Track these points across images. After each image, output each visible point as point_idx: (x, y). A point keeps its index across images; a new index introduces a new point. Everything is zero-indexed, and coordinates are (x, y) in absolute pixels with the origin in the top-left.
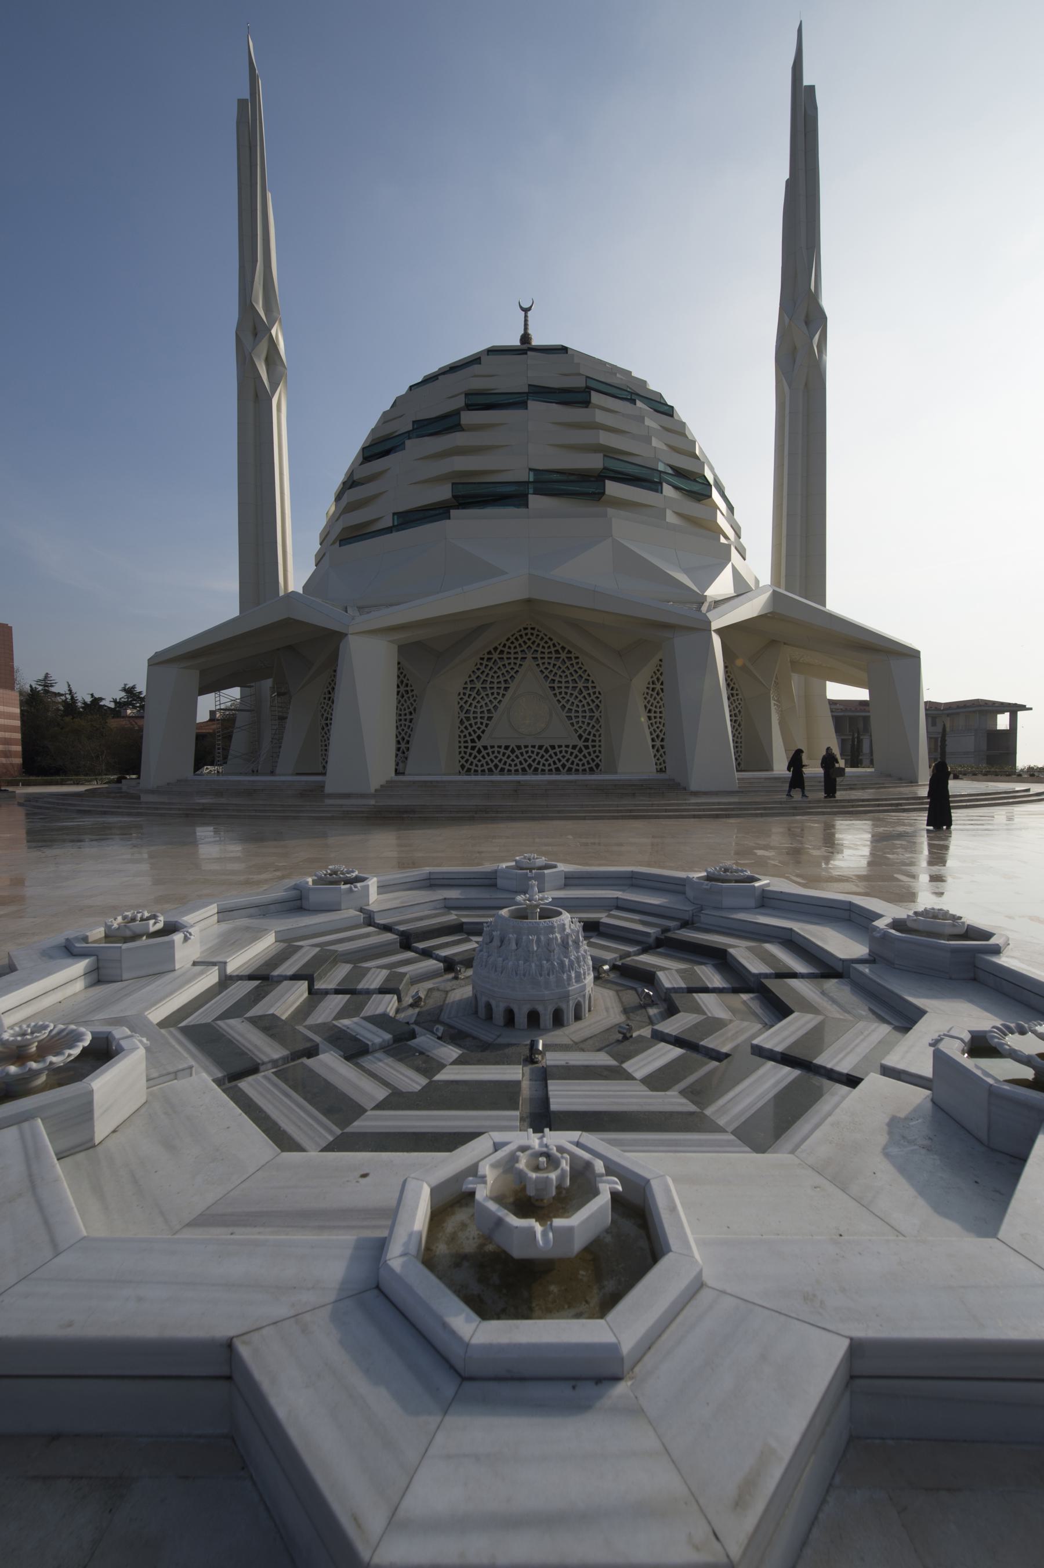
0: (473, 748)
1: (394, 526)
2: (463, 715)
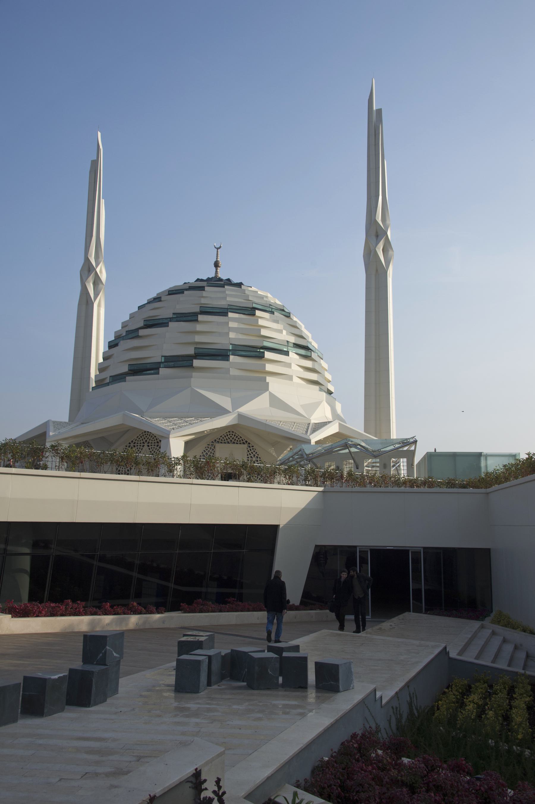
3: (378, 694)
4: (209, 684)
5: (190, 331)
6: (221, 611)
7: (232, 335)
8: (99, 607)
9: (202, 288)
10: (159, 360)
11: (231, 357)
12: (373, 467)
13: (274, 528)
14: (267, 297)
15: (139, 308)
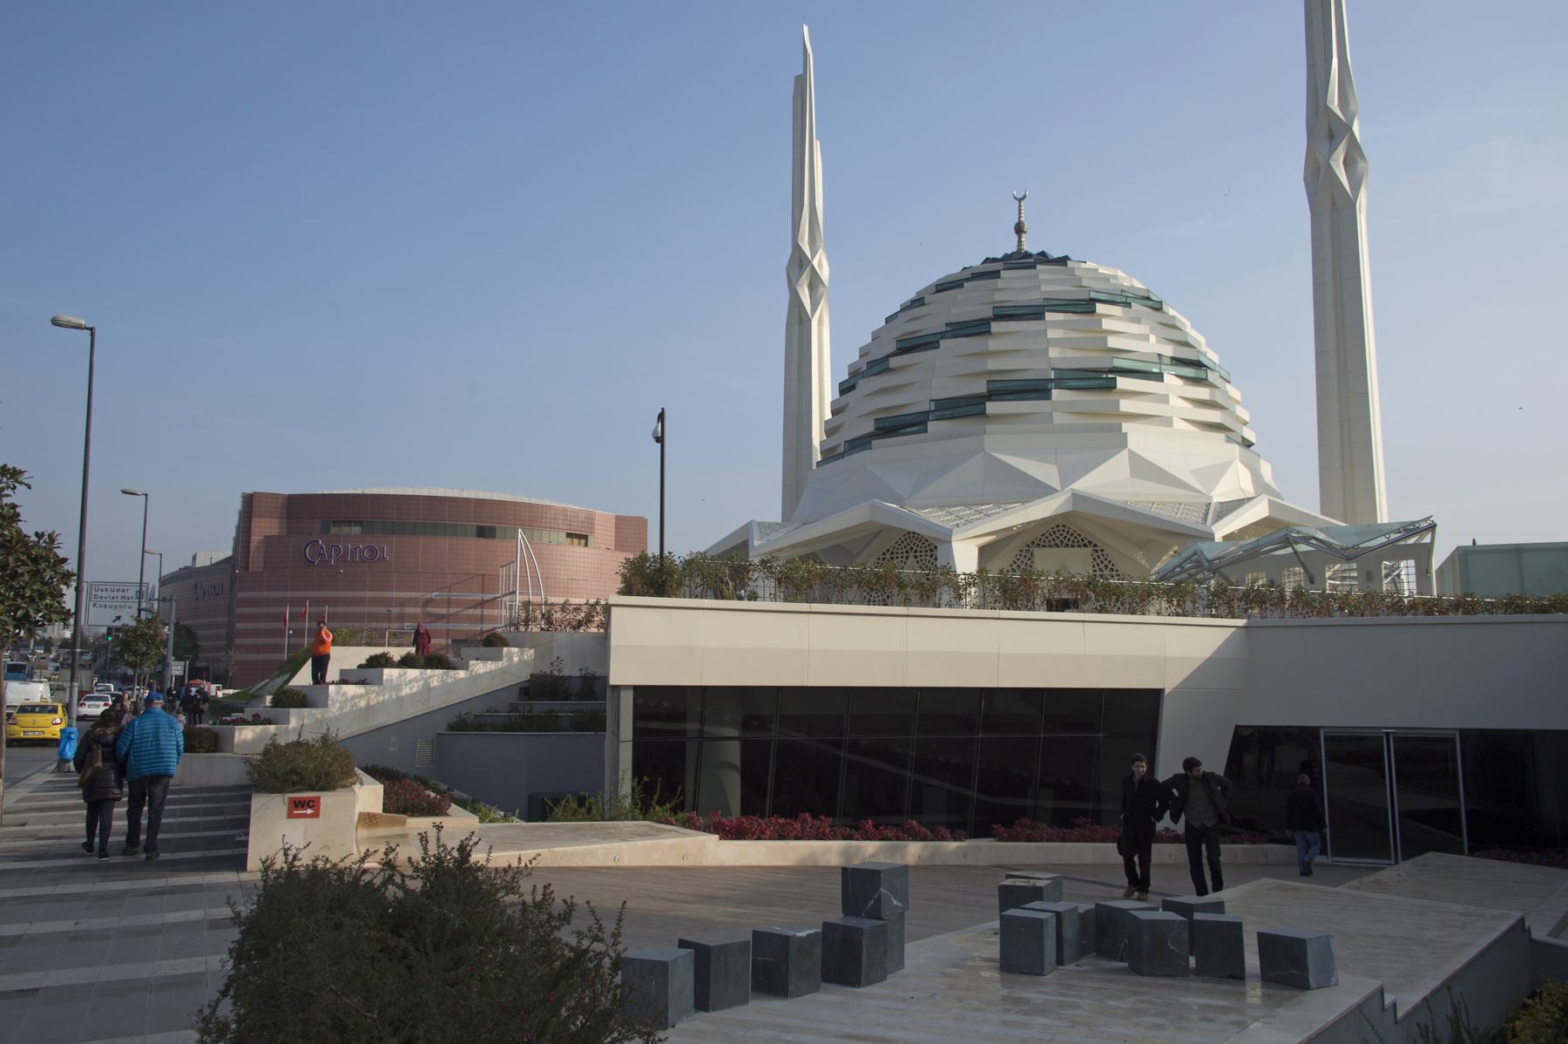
3: (1388, 999)
4: (1060, 961)
5: (980, 351)
6: (1064, 840)
7: (1054, 353)
8: (857, 828)
9: (995, 275)
10: (925, 407)
11: (1055, 392)
12: (1344, 578)
13: (1156, 694)
14: (1116, 277)
15: (888, 320)
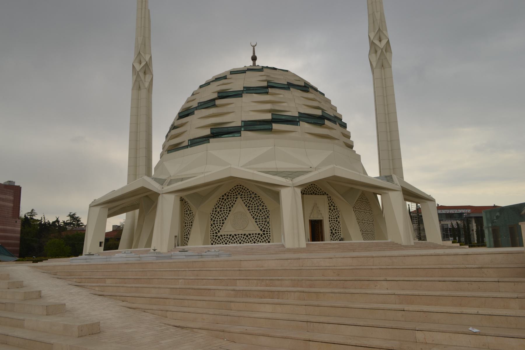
0: (216, 236)
1: (189, 145)
2: (268, 220)
10: (239, 124)
